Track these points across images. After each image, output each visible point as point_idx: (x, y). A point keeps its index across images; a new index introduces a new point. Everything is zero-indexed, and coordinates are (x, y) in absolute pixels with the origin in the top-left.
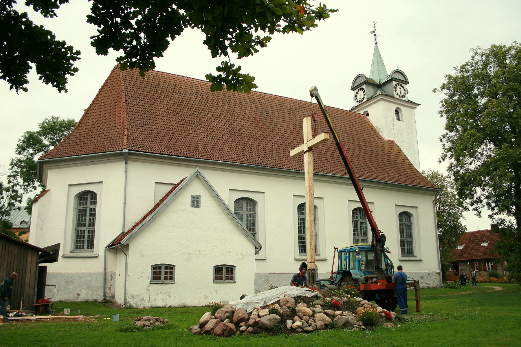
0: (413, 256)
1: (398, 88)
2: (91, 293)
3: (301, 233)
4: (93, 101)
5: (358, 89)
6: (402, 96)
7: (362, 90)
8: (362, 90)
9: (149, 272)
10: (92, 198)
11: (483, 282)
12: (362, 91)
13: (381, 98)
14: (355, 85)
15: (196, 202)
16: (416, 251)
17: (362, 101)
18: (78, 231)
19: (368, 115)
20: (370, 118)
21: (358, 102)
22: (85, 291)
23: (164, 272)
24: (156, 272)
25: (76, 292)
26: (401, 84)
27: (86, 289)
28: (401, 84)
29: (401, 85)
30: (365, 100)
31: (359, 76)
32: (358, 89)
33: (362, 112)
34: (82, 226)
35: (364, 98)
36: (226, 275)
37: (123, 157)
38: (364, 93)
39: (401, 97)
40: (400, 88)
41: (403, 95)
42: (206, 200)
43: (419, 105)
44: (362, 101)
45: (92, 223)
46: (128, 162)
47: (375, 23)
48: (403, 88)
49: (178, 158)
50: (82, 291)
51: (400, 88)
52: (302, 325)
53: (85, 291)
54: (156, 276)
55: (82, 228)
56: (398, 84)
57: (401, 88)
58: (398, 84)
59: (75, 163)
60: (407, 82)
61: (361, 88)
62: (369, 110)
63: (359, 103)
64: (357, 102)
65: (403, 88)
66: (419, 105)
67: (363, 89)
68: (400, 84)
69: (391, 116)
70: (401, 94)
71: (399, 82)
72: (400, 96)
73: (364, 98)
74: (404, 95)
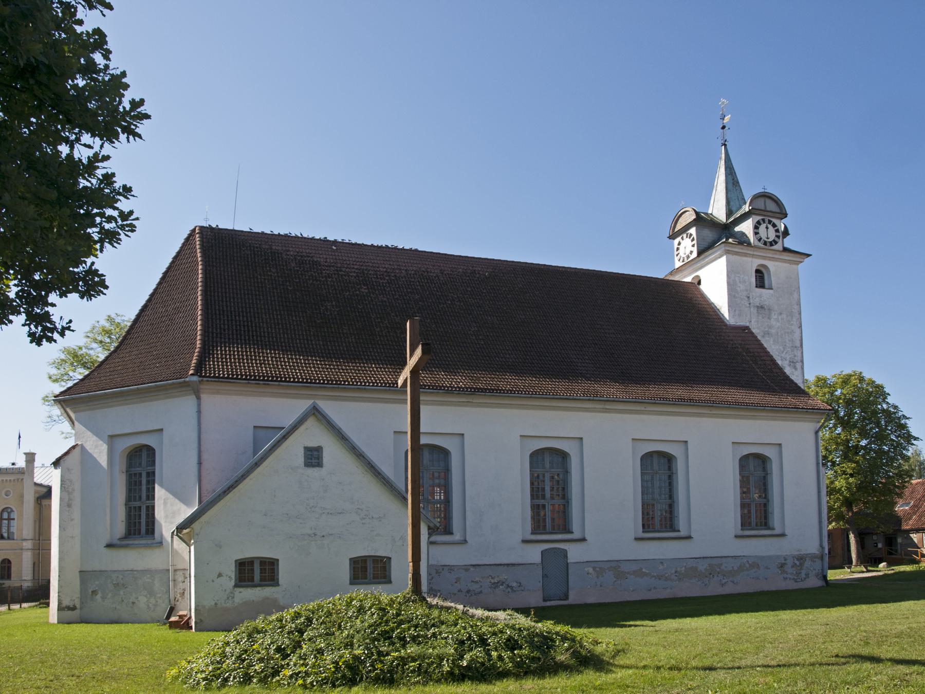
0: (769, 528)
1: (762, 228)
2: (154, 602)
3: (538, 498)
4: (152, 295)
6: (771, 243)
7: (690, 238)
8: (690, 238)
9: (231, 571)
10: (148, 455)
12: (688, 239)
14: (679, 227)
15: (313, 457)
16: (776, 521)
17: (688, 257)
19: (699, 283)
20: (703, 287)
21: (681, 260)
22: (145, 600)
23: (259, 570)
24: (265, 569)
25: (131, 600)
27: (146, 596)
29: (770, 222)
33: (688, 279)
34: (135, 500)
35: (691, 252)
36: (374, 571)
37: (190, 388)
39: (768, 244)
40: (767, 228)
41: (774, 241)
42: (332, 451)
43: (809, 255)
44: (688, 257)
48: (774, 225)
49: (92, 395)
50: (140, 598)
51: (767, 228)
53: (145, 600)
54: (248, 576)
55: (137, 504)
57: (770, 226)
58: (763, 220)
59: (262, 390)
60: (783, 214)
62: (703, 274)
65: (774, 225)
66: (809, 255)
67: (691, 235)
68: (767, 219)
69: (745, 282)
70: (768, 238)
71: (765, 216)
72: (765, 243)
73: (691, 252)
74: (777, 239)
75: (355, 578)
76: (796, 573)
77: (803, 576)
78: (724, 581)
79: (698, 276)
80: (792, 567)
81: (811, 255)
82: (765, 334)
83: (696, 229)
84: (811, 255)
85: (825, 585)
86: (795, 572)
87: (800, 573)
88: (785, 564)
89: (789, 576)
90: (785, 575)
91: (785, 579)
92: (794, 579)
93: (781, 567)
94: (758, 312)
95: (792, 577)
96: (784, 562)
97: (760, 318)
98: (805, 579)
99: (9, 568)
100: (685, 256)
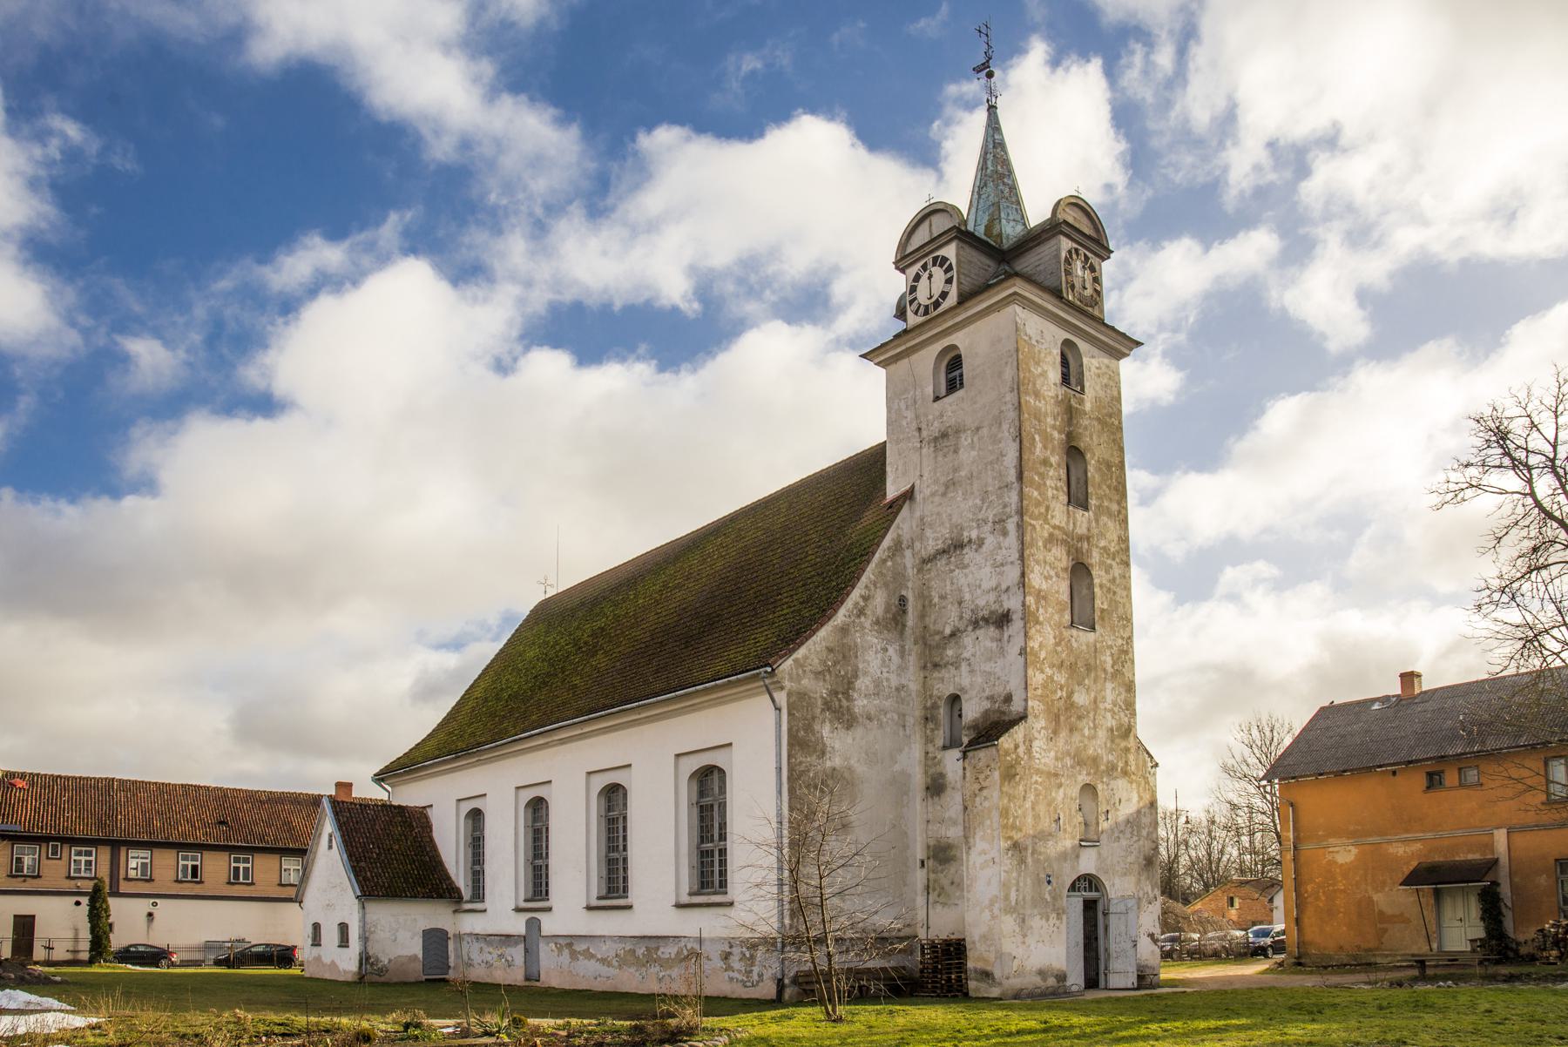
5: (922, 262)
7: (941, 266)
11: (1342, 967)
13: (1015, 293)
14: (909, 249)
17: (937, 304)
18: (702, 852)
21: (922, 310)
26: (1087, 253)
28: (1087, 253)
30: (952, 300)
31: (931, 209)
32: (922, 262)
35: (944, 295)
38: (949, 275)
44: (937, 304)
45: (726, 866)
46: (250, 375)
47: (984, 30)
52: (575, 204)
56: (1076, 250)
61: (935, 259)
63: (926, 313)
64: (916, 313)
73: (944, 295)
75: (609, 890)
76: (746, 971)
77: (756, 977)
78: (661, 974)
79: (953, 347)
80: (741, 960)
81: (1143, 344)
82: (947, 487)
83: (958, 249)
84: (1143, 344)
85: (1076, 979)
86: (743, 969)
87: (752, 971)
88: (730, 953)
89: (735, 975)
90: (731, 974)
91: (731, 979)
92: (742, 981)
93: (726, 958)
94: (936, 449)
95: (740, 979)
96: (729, 950)
97: (940, 459)
98: (758, 982)
99: (381, 772)
100: (928, 302)
